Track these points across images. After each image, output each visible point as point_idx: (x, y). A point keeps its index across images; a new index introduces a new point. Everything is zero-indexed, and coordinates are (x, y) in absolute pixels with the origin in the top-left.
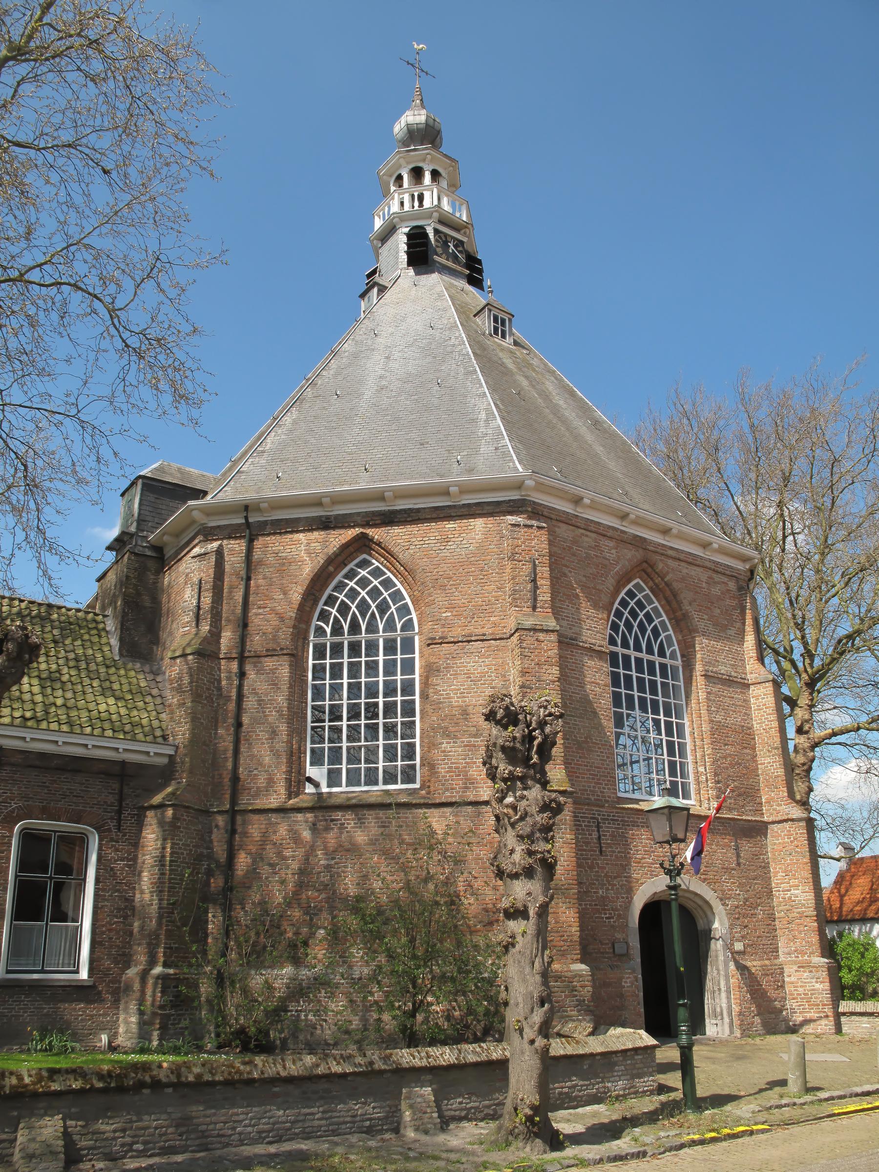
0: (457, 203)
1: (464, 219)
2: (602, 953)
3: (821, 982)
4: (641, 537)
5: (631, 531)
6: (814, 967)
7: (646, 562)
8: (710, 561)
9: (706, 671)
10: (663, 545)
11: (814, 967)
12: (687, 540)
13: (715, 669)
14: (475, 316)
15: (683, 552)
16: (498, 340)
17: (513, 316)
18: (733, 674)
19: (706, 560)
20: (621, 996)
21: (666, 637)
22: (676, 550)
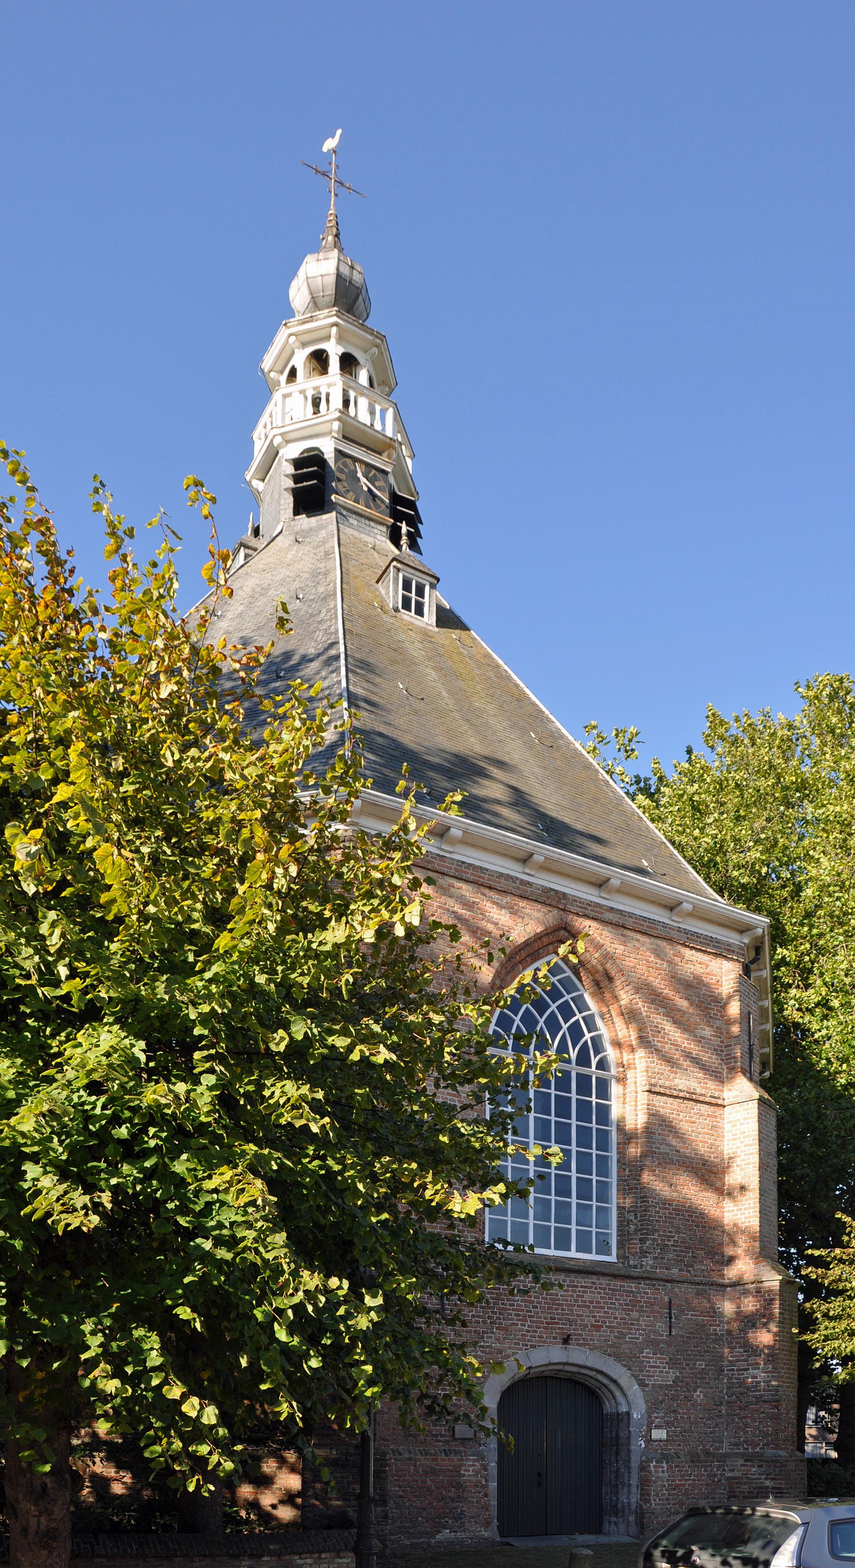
0: (378, 408)
1: (389, 433)
2: (436, 1436)
3: (772, 1479)
4: (556, 892)
5: (541, 882)
6: (765, 1461)
7: (565, 929)
8: (679, 930)
9: (651, 1085)
10: (598, 905)
11: (765, 1461)
12: (484, 849)
13: (667, 1084)
14: (378, 582)
15: (631, 915)
16: (409, 616)
17: (438, 580)
18: (698, 1091)
19: (672, 928)
20: (459, 1486)
21: (592, 1038)
22: (621, 912)
